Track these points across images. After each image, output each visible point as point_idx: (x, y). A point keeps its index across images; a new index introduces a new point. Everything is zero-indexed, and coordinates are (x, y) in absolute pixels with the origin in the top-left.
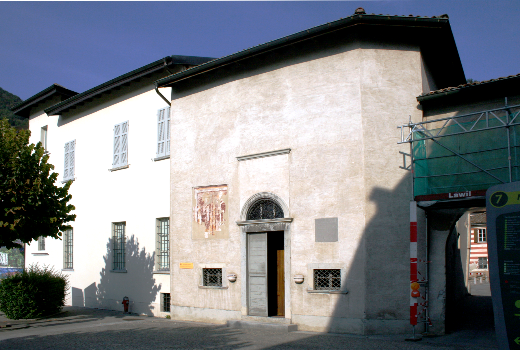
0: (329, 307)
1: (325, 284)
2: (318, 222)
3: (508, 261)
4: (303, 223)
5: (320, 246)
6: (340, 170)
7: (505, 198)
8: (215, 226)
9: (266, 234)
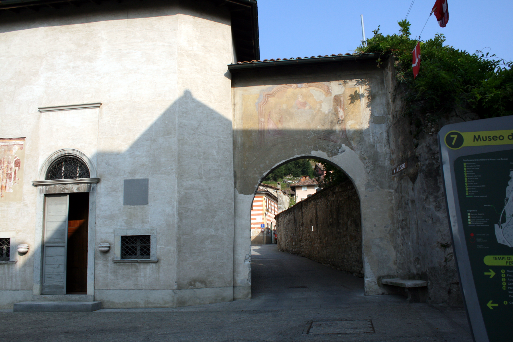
0: (138, 279)
1: (133, 252)
2: (127, 183)
3: (472, 211)
4: (111, 184)
5: (129, 210)
6: (153, 129)
7: (460, 140)
8: (5, 186)
9: (68, 196)
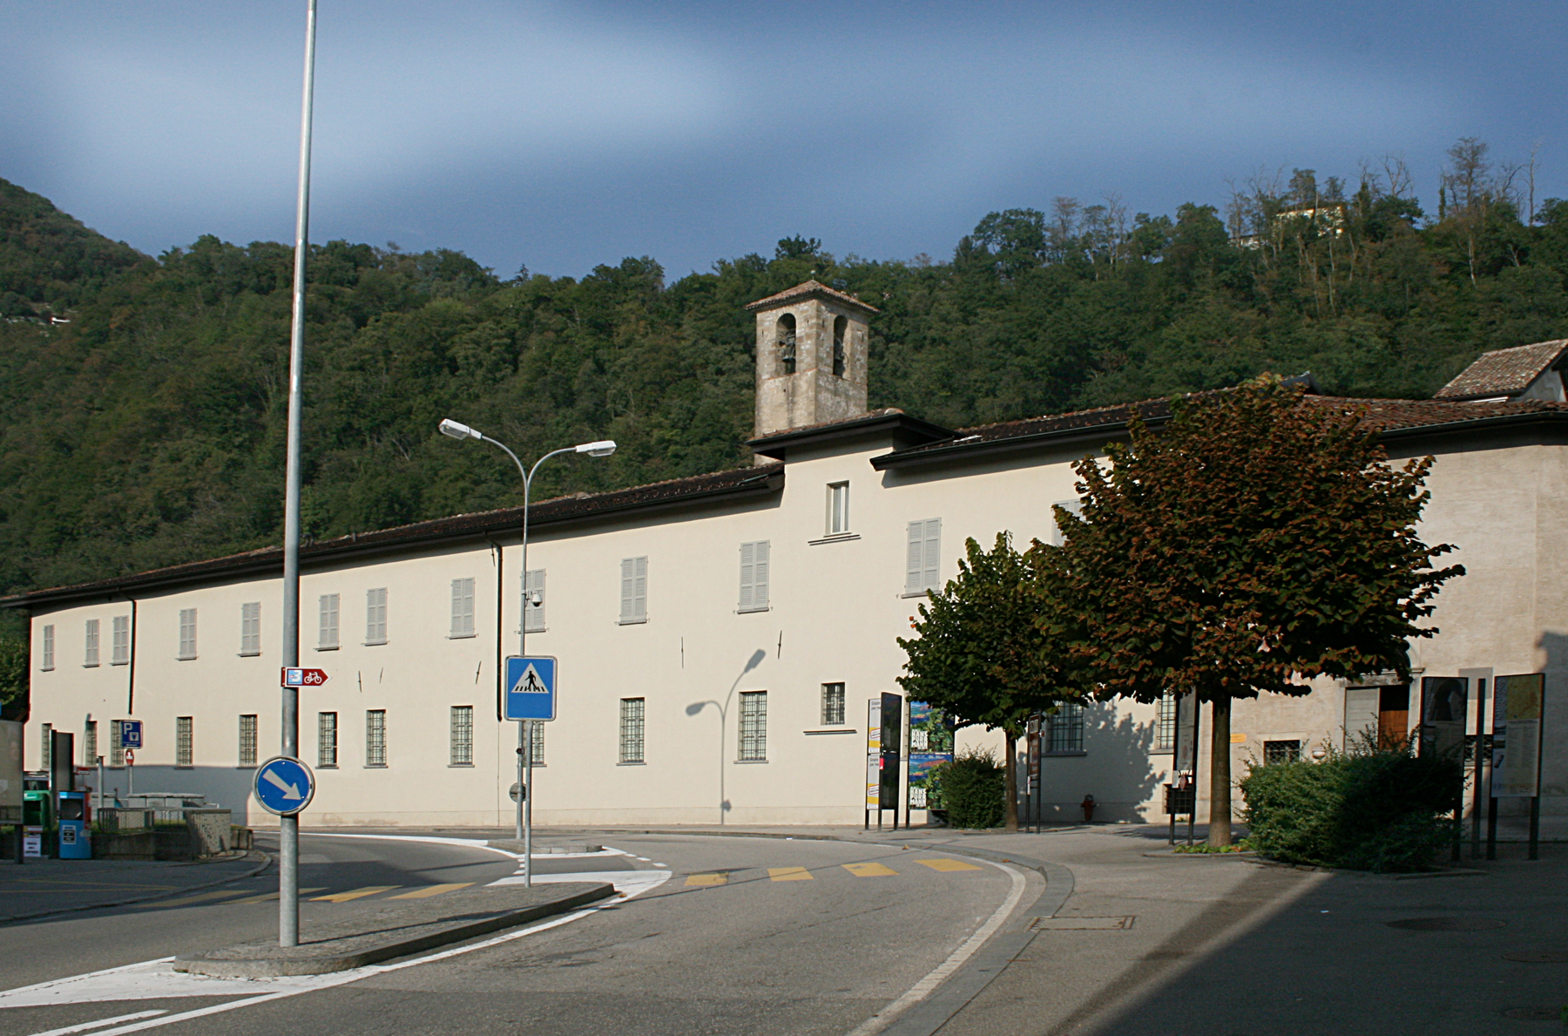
9: (1379, 689)
